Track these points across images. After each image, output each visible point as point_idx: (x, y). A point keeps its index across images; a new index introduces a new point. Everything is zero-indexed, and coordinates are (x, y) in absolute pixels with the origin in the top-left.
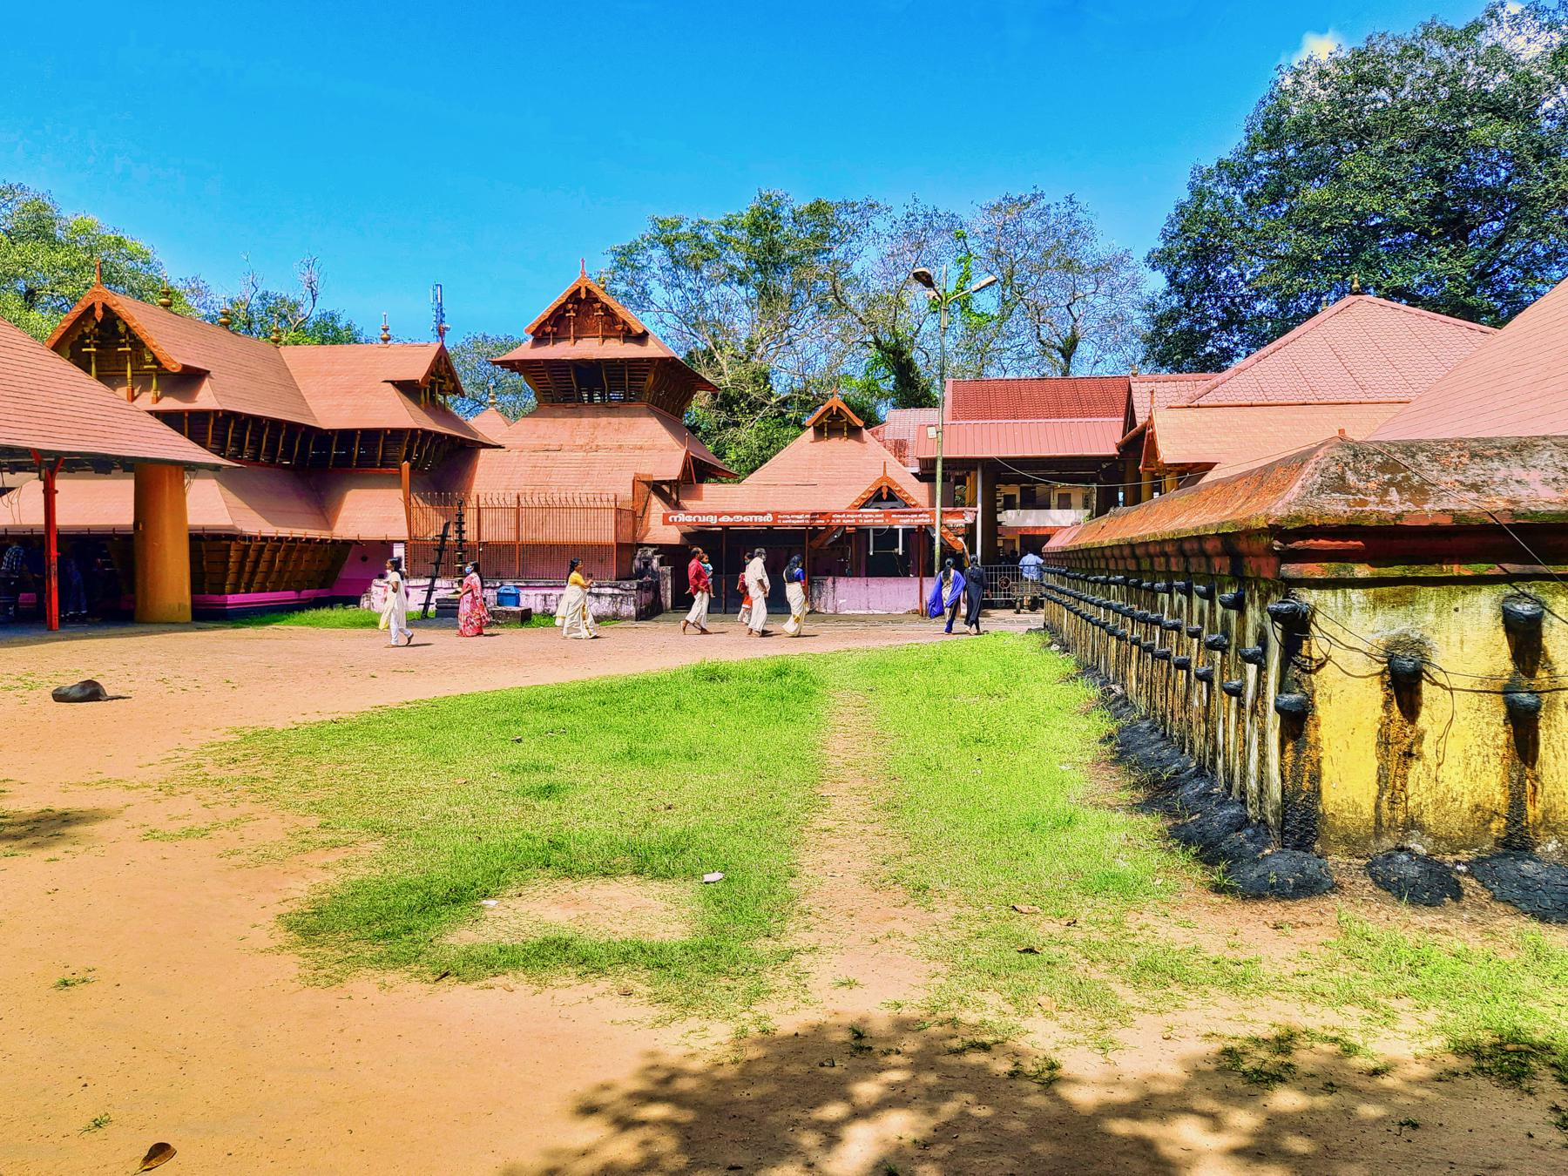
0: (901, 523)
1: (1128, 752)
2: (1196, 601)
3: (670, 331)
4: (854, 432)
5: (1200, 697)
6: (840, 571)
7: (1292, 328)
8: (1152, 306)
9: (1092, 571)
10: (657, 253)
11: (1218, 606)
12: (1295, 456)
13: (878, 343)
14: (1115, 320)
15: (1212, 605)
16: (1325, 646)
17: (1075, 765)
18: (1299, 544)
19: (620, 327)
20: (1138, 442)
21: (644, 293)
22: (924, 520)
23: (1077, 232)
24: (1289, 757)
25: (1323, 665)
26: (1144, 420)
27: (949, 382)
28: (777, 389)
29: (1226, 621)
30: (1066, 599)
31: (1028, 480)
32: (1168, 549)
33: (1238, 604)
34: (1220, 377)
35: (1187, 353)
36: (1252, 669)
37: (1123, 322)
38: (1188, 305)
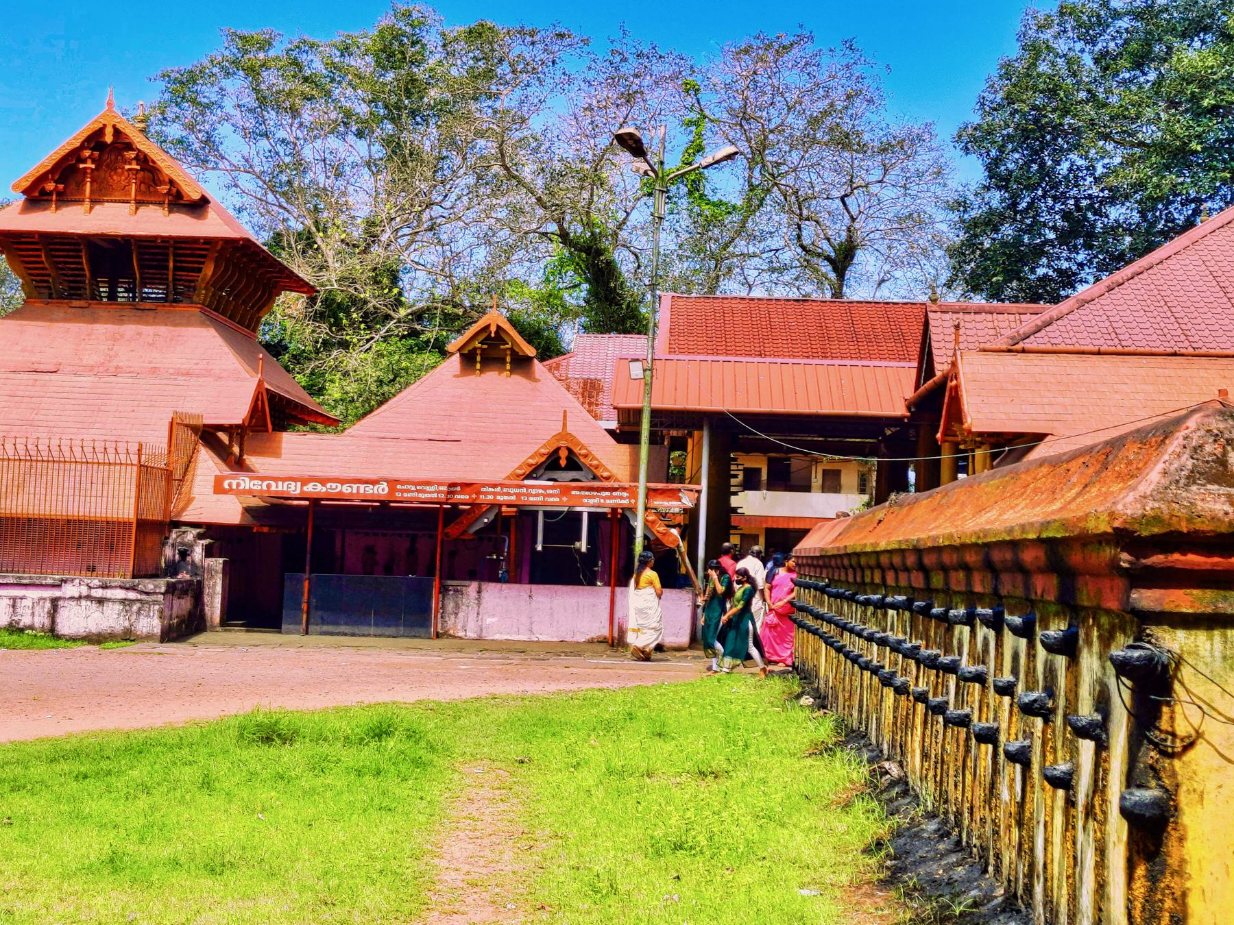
0: (587, 504)
1: (904, 870)
2: (1009, 638)
3: (247, 200)
4: (521, 364)
5: (1011, 787)
6: (488, 574)
7: (1159, 245)
8: (961, 205)
9: (862, 586)
10: (237, 85)
11: (1040, 647)
12: (1155, 428)
13: (564, 236)
14: (911, 221)
15: (1031, 646)
16: (1195, 716)
17: (823, 887)
18: (1157, 559)
19: (164, 189)
20: (936, 400)
21: (209, 141)
22: (621, 500)
23: (858, 93)
24: (1140, 886)
25: (1191, 745)
26: (946, 367)
27: (667, 297)
28: (410, 296)
29: (1050, 672)
30: (825, 628)
31: (777, 448)
32: (971, 558)
33: (1068, 647)
34: (1052, 310)
35: (1012, 274)
36: (1087, 747)
37: (920, 224)
38: (1013, 206)
